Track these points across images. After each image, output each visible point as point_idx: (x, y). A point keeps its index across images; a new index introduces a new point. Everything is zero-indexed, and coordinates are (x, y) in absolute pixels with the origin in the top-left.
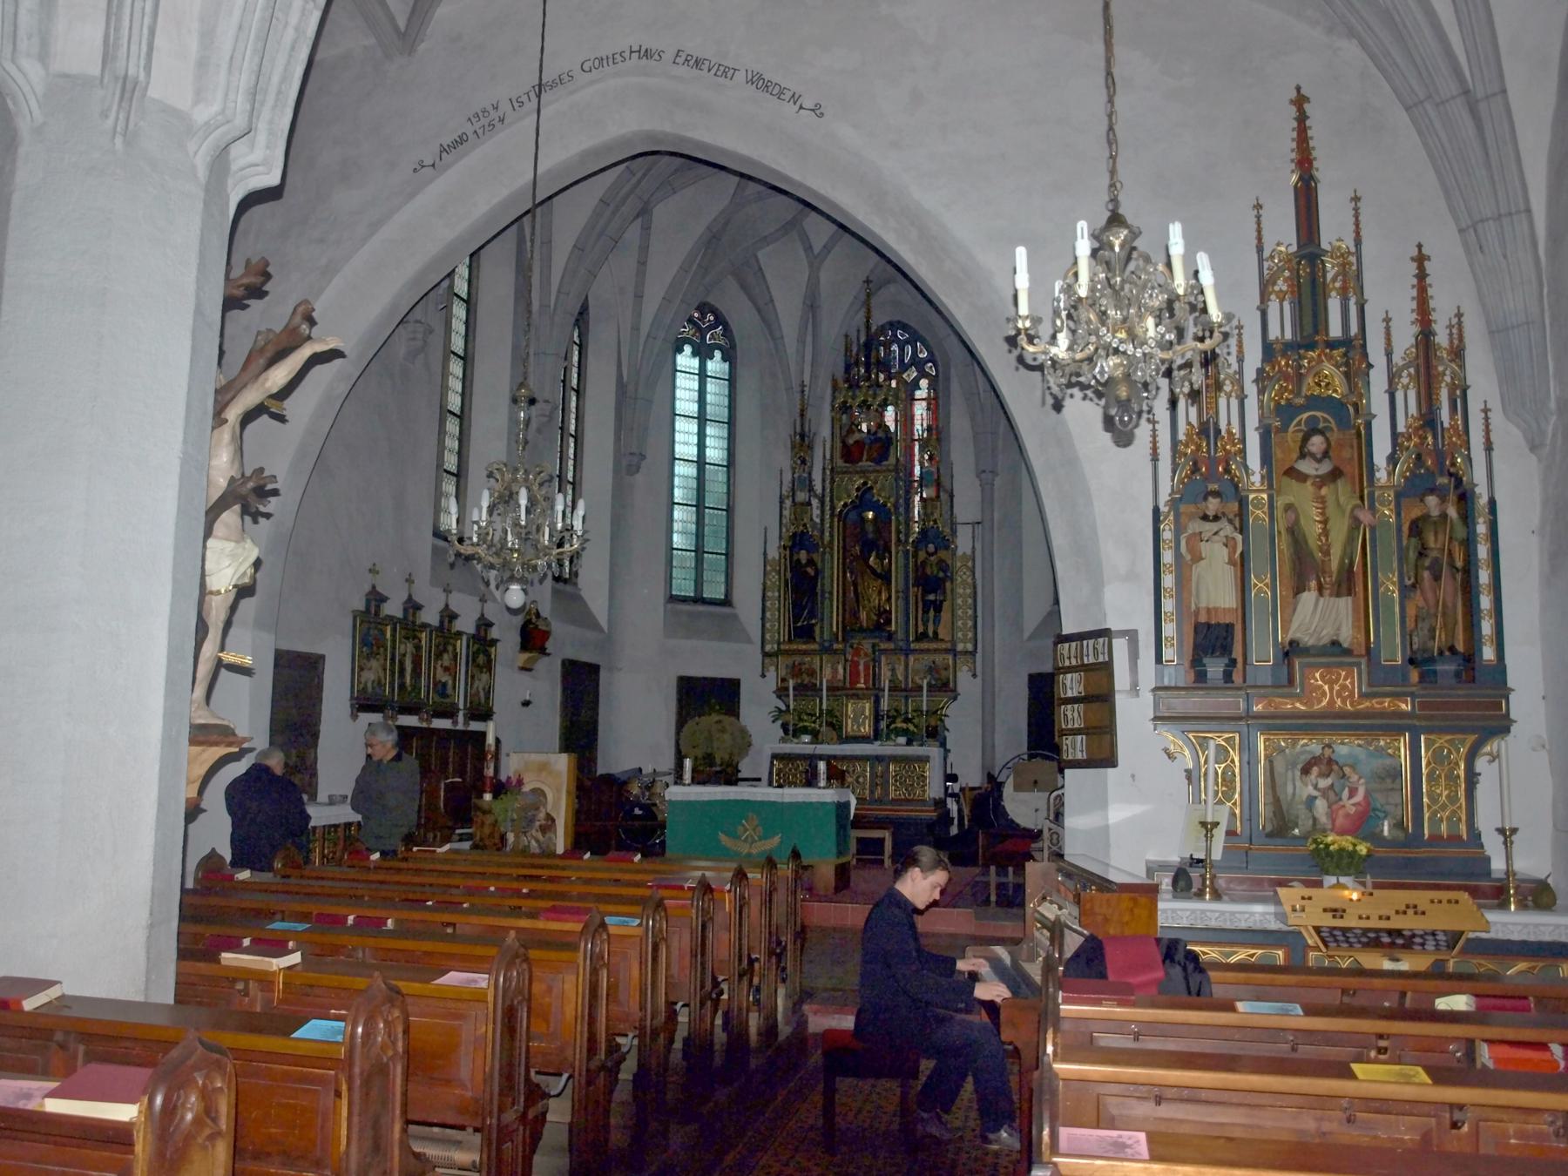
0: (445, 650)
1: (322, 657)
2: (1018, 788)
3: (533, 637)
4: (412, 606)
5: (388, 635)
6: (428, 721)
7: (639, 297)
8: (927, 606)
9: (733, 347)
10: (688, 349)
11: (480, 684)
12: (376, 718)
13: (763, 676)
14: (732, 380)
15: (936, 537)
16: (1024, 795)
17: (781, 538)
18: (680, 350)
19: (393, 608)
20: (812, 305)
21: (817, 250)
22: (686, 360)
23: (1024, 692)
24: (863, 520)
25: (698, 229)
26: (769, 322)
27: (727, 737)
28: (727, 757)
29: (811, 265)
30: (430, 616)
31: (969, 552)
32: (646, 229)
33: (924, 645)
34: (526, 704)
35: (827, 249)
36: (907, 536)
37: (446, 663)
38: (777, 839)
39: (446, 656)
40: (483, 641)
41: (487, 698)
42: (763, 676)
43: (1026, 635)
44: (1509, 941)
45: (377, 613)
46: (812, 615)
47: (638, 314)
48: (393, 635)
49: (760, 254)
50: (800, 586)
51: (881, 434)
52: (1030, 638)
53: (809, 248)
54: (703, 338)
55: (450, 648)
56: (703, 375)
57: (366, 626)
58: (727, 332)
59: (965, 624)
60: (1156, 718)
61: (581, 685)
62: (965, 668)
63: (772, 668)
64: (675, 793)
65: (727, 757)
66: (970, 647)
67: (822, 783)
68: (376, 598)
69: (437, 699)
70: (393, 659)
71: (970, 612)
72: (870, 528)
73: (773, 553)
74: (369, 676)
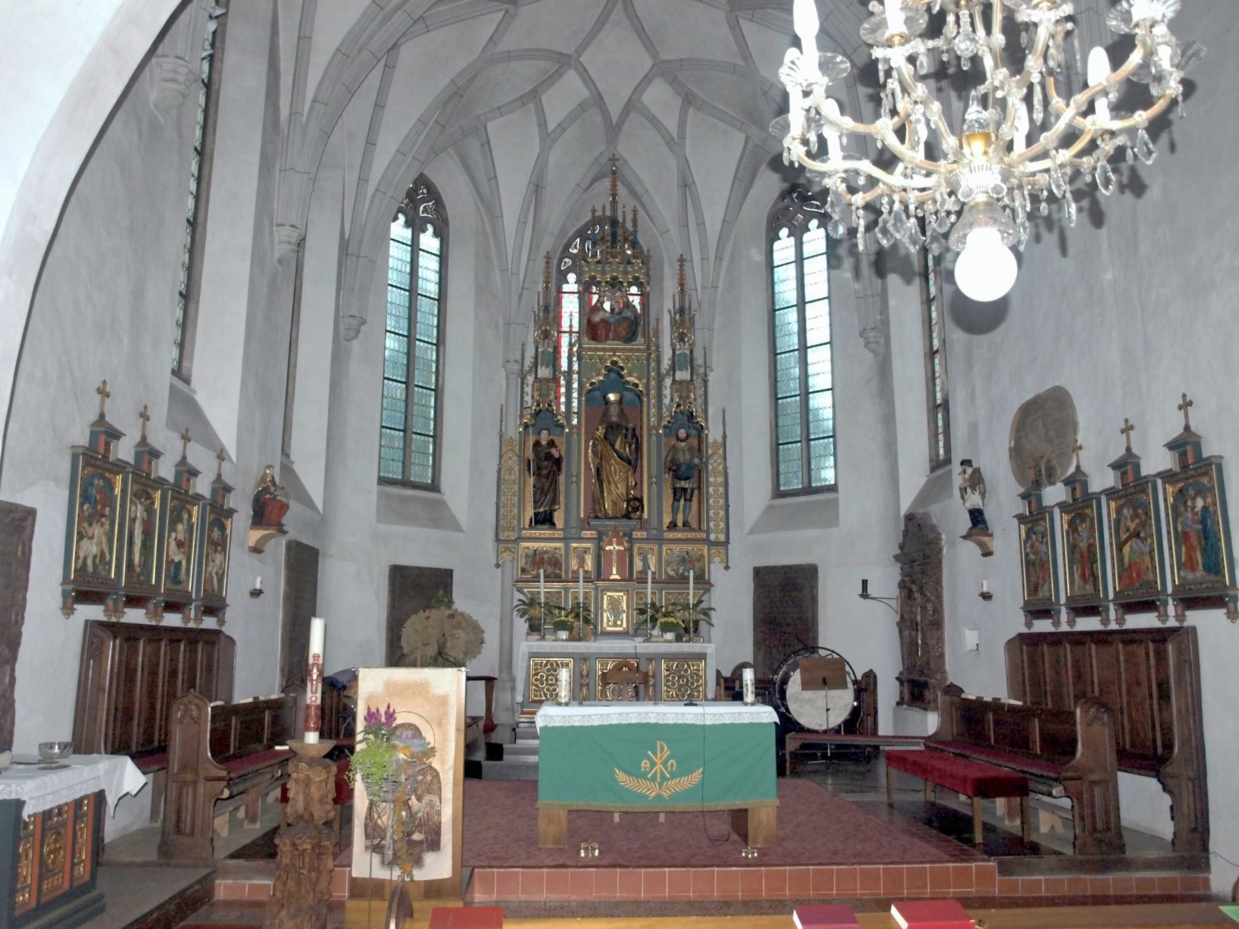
0: (180, 520)
1: (32, 513)
2: (807, 685)
3: (266, 510)
4: (147, 452)
5: (118, 491)
6: (117, 611)
7: (370, 143)
8: (678, 493)
9: (445, 221)
11: (213, 569)
12: (95, 612)
14: (443, 257)
15: (689, 423)
16: (808, 694)
18: (395, 219)
19: (124, 451)
20: (537, 188)
21: (551, 126)
22: (399, 230)
23: (750, 585)
24: (607, 402)
25: (442, 81)
26: (489, 204)
29: (542, 139)
30: (165, 469)
31: (720, 440)
32: (389, 68)
33: (671, 535)
34: (986, 596)
35: (562, 127)
37: (181, 537)
38: (697, 776)
39: (180, 527)
40: (219, 514)
41: (220, 580)
43: (748, 527)
44: (611, 725)
45: (105, 457)
47: (366, 165)
48: (124, 491)
49: (490, 126)
51: (628, 313)
52: (752, 532)
53: (543, 124)
54: (416, 209)
55: (185, 516)
56: (415, 247)
57: (90, 470)
58: (439, 203)
59: (716, 514)
61: (303, 568)
62: (717, 560)
64: (549, 716)
66: (722, 538)
67: (750, 697)
68: (105, 432)
69: (170, 586)
70: (121, 525)
71: (722, 501)
72: (614, 410)
74: (90, 548)
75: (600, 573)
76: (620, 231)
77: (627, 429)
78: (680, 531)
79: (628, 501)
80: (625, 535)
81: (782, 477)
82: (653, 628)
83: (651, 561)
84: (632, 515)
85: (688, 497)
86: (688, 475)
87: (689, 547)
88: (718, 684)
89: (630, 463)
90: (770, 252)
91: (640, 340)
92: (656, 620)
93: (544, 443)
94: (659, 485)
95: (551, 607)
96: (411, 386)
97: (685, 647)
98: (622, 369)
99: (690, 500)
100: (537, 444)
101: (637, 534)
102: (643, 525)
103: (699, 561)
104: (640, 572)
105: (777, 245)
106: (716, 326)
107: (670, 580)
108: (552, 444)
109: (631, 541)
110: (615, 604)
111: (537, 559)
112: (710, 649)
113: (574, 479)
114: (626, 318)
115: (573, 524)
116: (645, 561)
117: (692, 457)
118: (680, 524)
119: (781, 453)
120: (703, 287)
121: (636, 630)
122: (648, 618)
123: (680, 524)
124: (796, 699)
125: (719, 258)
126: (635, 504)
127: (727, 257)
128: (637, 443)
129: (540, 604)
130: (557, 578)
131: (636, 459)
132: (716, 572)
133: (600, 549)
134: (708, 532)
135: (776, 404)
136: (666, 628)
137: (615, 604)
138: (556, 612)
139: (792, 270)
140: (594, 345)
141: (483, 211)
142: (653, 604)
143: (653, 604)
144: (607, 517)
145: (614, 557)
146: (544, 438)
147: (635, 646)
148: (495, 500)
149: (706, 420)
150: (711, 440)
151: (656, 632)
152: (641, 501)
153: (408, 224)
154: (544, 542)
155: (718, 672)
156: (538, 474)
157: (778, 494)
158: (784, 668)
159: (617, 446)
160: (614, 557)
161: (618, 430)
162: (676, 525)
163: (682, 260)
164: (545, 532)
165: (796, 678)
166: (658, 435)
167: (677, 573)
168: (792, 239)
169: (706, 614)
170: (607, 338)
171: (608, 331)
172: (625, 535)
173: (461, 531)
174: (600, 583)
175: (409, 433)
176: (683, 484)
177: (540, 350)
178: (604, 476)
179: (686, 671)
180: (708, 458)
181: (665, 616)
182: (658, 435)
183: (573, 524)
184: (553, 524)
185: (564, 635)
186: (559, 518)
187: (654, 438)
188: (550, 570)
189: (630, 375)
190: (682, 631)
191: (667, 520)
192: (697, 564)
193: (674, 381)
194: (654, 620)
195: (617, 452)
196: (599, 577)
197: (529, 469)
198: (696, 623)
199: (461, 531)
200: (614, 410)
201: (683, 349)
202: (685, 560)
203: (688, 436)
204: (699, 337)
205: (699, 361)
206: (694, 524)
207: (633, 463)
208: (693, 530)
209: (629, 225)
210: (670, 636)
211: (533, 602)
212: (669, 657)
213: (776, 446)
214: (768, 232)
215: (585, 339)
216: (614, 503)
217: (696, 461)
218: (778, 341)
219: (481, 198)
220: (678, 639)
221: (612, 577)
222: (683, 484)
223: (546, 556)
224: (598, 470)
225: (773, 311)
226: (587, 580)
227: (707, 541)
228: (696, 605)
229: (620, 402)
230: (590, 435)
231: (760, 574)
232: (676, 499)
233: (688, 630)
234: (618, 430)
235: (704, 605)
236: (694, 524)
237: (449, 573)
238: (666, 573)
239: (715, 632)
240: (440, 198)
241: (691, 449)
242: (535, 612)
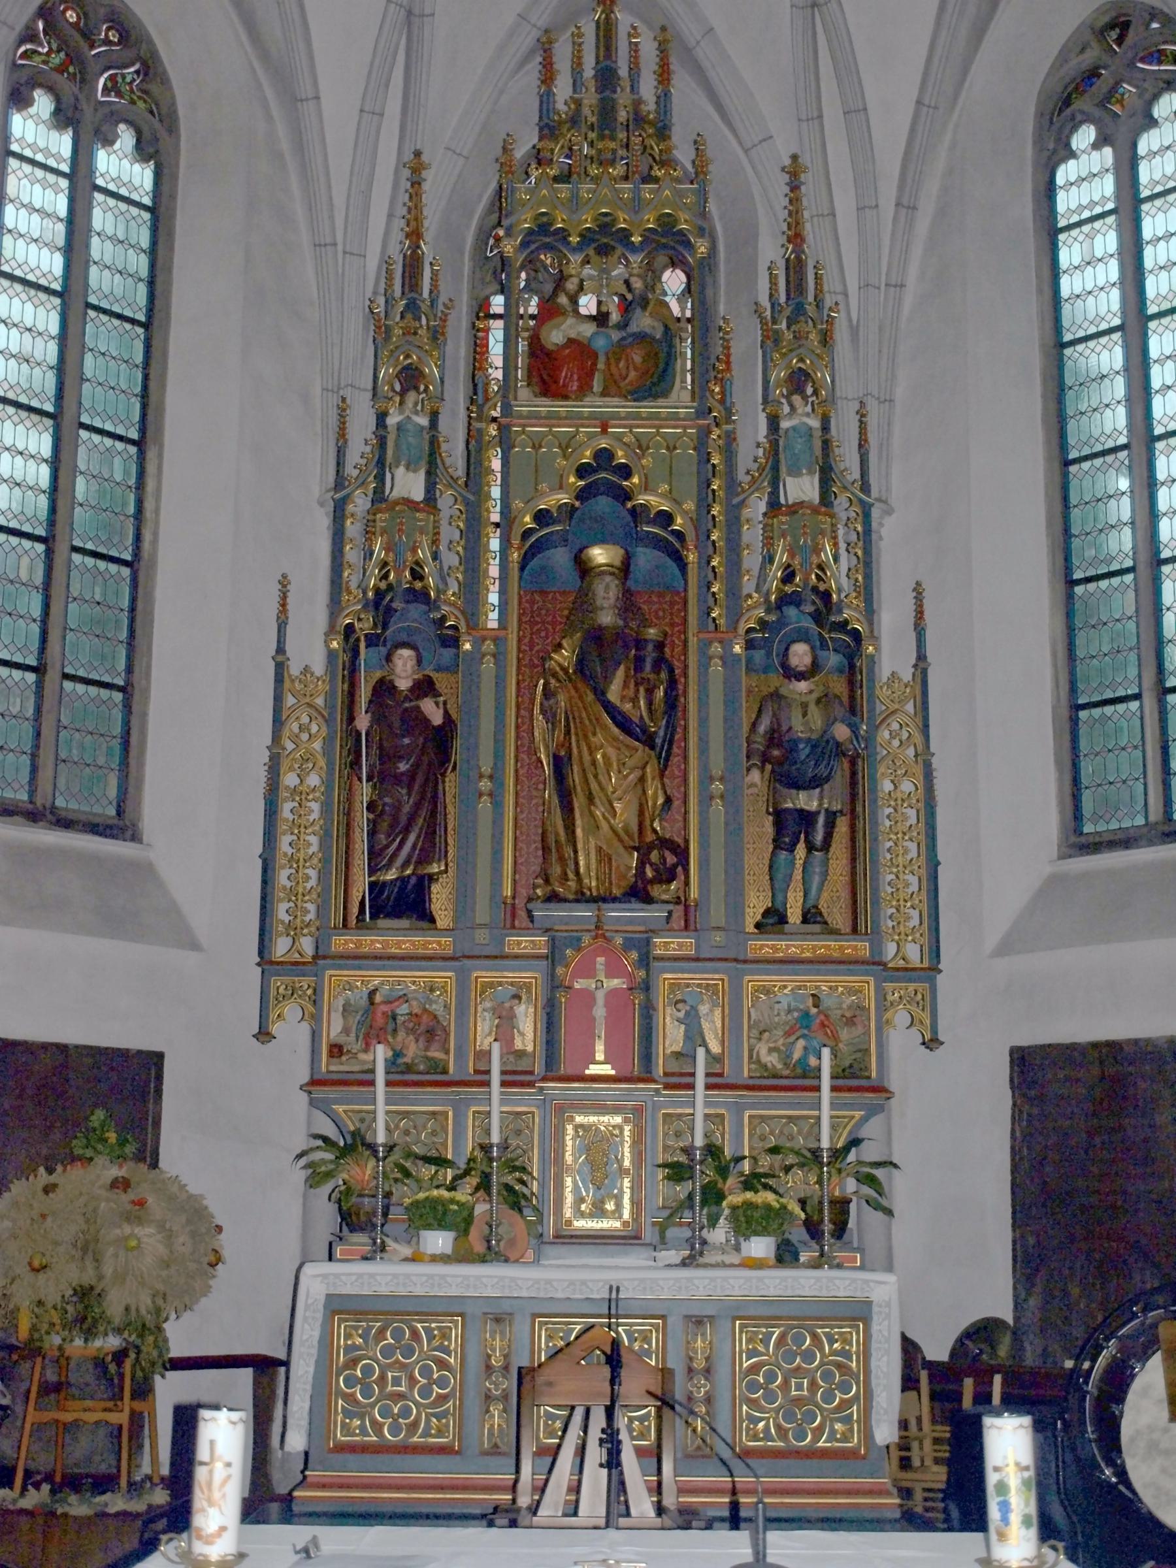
8: (790, 828)
9: (170, 121)
10: (43, 104)
13: (264, 1034)
14: (159, 211)
15: (824, 624)
17: (335, 604)
22: (33, 128)
24: (584, 568)
27: (147, 1234)
28: (145, 1302)
31: (907, 674)
33: (767, 946)
36: (735, 615)
42: (264, 1034)
43: (992, 940)
46: (427, 852)
50: (395, 757)
51: (643, 322)
52: (1005, 948)
56: (80, 180)
58: (150, 68)
60: (315, 1082)
62: (901, 1017)
63: (292, 1010)
65: (145, 1302)
66: (913, 953)
72: (606, 594)
73: (312, 649)
75: (554, 1062)
76: (623, 98)
77: (640, 643)
78: (792, 935)
79: (644, 851)
80: (628, 945)
81: (1087, 797)
82: (713, 1222)
83: (701, 1019)
84: (656, 891)
85: (819, 837)
86: (821, 779)
87: (822, 982)
88: (909, 1383)
89: (648, 740)
90: (1049, 191)
91: (681, 396)
92: (720, 1197)
93: (403, 684)
94: (731, 798)
95: (405, 1161)
96: (61, 548)
97: (805, 1283)
98: (625, 471)
99: (826, 845)
100: (384, 689)
101: (667, 944)
102: (688, 916)
103: (850, 1022)
104: (678, 1055)
105: (1066, 172)
106: (900, 393)
107: (767, 1083)
108: (424, 687)
109: (645, 960)
110: (598, 1148)
111: (375, 1021)
112: (881, 1288)
113: (485, 785)
114: (642, 338)
115: (482, 913)
116: (691, 1021)
117: (830, 723)
118: (794, 915)
119: (1083, 730)
120: (864, 286)
121: (662, 1228)
122: (702, 1188)
123: (794, 915)
124: (1153, 1448)
125: (906, 206)
126: (658, 865)
127: (931, 189)
128: (672, 683)
129: (372, 1148)
130: (436, 1076)
131: (671, 727)
132: (900, 1051)
133: (554, 985)
134: (876, 937)
135: (1070, 597)
136: (749, 1222)
137: (598, 1148)
138: (427, 1171)
139: (1107, 240)
140: (545, 406)
141: (269, 93)
142: (712, 1150)
143: (712, 1150)
144: (581, 898)
145: (600, 1012)
146: (404, 669)
147: (651, 1278)
148: (257, 845)
149: (870, 613)
150: (884, 671)
151: (719, 1234)
152: (682, 853)
153: (63, 117)
154: (400, 966)
155: (909, 1347)
156: (382, 778)
157: (1080, 842)
158: (1110, 1351)
159: (614, 693)
160: (600, 1012)
161: (617, 656)
162: (783, 920)
163: (794, 173)
164: (395, 937)
165: (1150, 1380)
166: (728, 660)
167: (786, 1058)
168: (1108, 151)
169: (871, 1181)
170: (585, 388)
171: (587, 376)
172: (628, 945)
173: (195, 946)
174: (553, 1087)
175: (52, 676)
176: (806, 801)
177: (392, 420)
178: (575, 776)
179: (808, 1356)
180: (875, 728)
181: (748, 1184)
182: (728, 660)
183: (482, 913)
184: (432, 920)
185: (439, 1241)
186: (440, 898)
187: (717, 667)
188: (413, 1050)
189: (646, 487)
190: (798, 1234)
191: (756, 904)
192: (845, 1034)
193: (774, 506)
194: (712, 1195)
195: (609, 707)
196: (552, 1072)
197: (355, 763)
198: (841, 1206)
199: (195, 946)
200: (606, 594)
201: (800, 418)
202: (812, 1021)
203: (815, 668)
204: (848, 373)
205: (847, 459)
206: (838, 917)
207: (659, 740)
208: (831, 932)
209: (648, 89)
210: (760, 1247)
211: (356, 1144)
212: (755, 1315)
213: (1074, 710)
214: (1039, 141)
215: (524, 393)
216: (604, 857)
217: (841, 732)
218: (1071, 426)
219: (265, 56)
220: (786, 1255)
221: (593, 1070)
222: (806, 801)
223: (403, 1009)
224: (560, 765)
225: (1057, 346)
226: (514, 1079)
227: (876, 963)
228: (838, 1154)
229: (625, 569)
230: (535, 662)
231: (1029, 1067)
232: (783, 839)
233: (825, 1228)
234: (617, 656)
235: (870, 1152)
236: (838, 917)
237: (160, 1056)
238: (754, 1059)
239: (906, 1232)
240: (154, 54)
241: (825, 700)
242: (363, 1172)
